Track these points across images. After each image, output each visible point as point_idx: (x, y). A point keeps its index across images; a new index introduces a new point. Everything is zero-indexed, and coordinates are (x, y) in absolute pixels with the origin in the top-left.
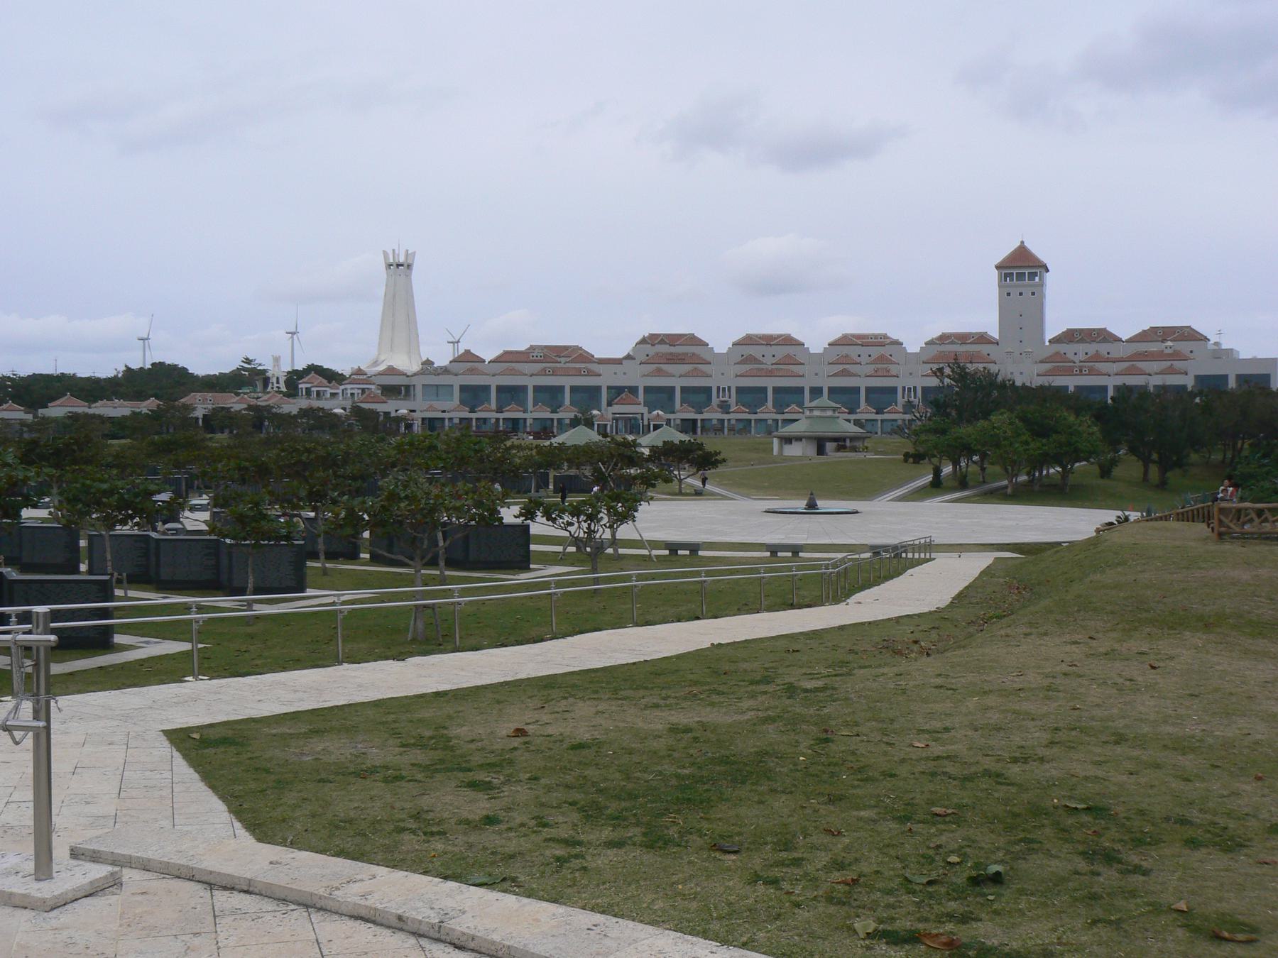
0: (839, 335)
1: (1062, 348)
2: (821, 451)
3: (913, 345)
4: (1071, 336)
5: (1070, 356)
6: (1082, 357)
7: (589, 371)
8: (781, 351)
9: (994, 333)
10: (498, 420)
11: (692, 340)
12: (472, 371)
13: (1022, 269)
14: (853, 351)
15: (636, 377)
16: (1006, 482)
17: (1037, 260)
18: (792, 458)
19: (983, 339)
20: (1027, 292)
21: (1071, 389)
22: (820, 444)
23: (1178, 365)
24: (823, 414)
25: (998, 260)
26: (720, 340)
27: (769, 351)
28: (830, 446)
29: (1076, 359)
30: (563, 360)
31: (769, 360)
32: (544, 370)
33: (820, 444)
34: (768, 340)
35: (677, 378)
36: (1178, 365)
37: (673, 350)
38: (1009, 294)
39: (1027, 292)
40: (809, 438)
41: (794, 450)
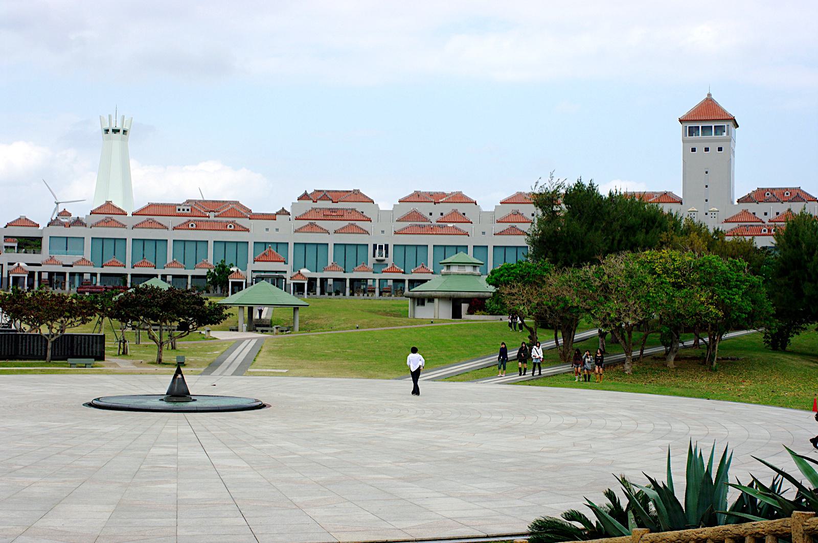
0: (513, 193)
1: (751, 207)
2: (457, 314)
3: (489, 199)
4: (761, 196)
5: (760, 215)
6: (772, 216)
7: (236, 225)
8: (447, 209)
9: (679, 193)
10: (94, 275)
11: (357, 196)
12: (107, 223)
13: (708, 123)
14: (424, 209)
15: (285, 232)
16: (624, 356)
17: (724, 112)
18: (422, 321)
19: (667, 197)
20: (713, 148)
21: (28, 288)
22: (456, 303)
23: (463, 227)
24: (462, 271)
25: (683, 113)
26: (386, 198)
27: (437, 210)
28: (465, 307)
29: (766, 219)
30: (212, 214)
31: (433, 220)
32: (186, 223)
33: (456, 303)
34: (435, 198)
35: (331, 235)
36: (463, 227)
37: (335, 206)
38: (693, 150)
39: (713, 148)
40: (441, 298)
41: (425, 312)
